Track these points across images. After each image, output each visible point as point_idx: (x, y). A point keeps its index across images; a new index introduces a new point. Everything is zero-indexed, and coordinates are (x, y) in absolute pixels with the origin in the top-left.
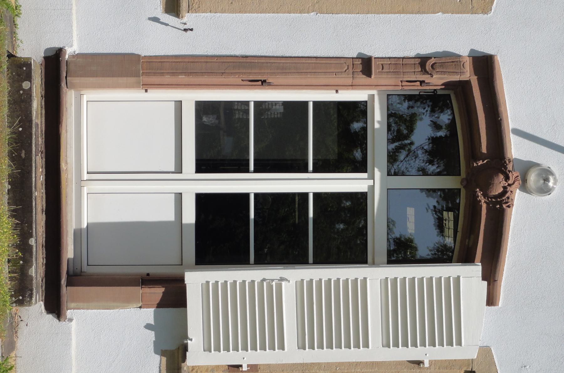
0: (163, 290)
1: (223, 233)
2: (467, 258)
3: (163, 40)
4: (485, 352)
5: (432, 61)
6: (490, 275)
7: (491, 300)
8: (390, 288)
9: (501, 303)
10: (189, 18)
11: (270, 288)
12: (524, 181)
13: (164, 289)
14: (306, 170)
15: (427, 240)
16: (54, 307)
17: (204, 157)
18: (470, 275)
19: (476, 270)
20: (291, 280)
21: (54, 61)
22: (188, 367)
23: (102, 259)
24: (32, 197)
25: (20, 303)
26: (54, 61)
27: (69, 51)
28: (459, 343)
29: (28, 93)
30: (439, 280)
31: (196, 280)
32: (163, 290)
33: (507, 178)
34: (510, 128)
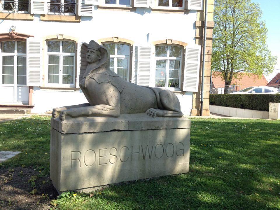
1: (22, 80)
6: (28, 37)
7: (33, 37)
8: (31, 52)
12: (14, 30)
13: (270, 103)
14: (59, 75)
15: (241, 107)
18: (28, 40)
19: (27, 39)
20: (29, 69)
22: (108, 88)
24: (256, 94)
28: (39, 42)
31: (29, 84)
33: (12, 33)
34: (196, 94)
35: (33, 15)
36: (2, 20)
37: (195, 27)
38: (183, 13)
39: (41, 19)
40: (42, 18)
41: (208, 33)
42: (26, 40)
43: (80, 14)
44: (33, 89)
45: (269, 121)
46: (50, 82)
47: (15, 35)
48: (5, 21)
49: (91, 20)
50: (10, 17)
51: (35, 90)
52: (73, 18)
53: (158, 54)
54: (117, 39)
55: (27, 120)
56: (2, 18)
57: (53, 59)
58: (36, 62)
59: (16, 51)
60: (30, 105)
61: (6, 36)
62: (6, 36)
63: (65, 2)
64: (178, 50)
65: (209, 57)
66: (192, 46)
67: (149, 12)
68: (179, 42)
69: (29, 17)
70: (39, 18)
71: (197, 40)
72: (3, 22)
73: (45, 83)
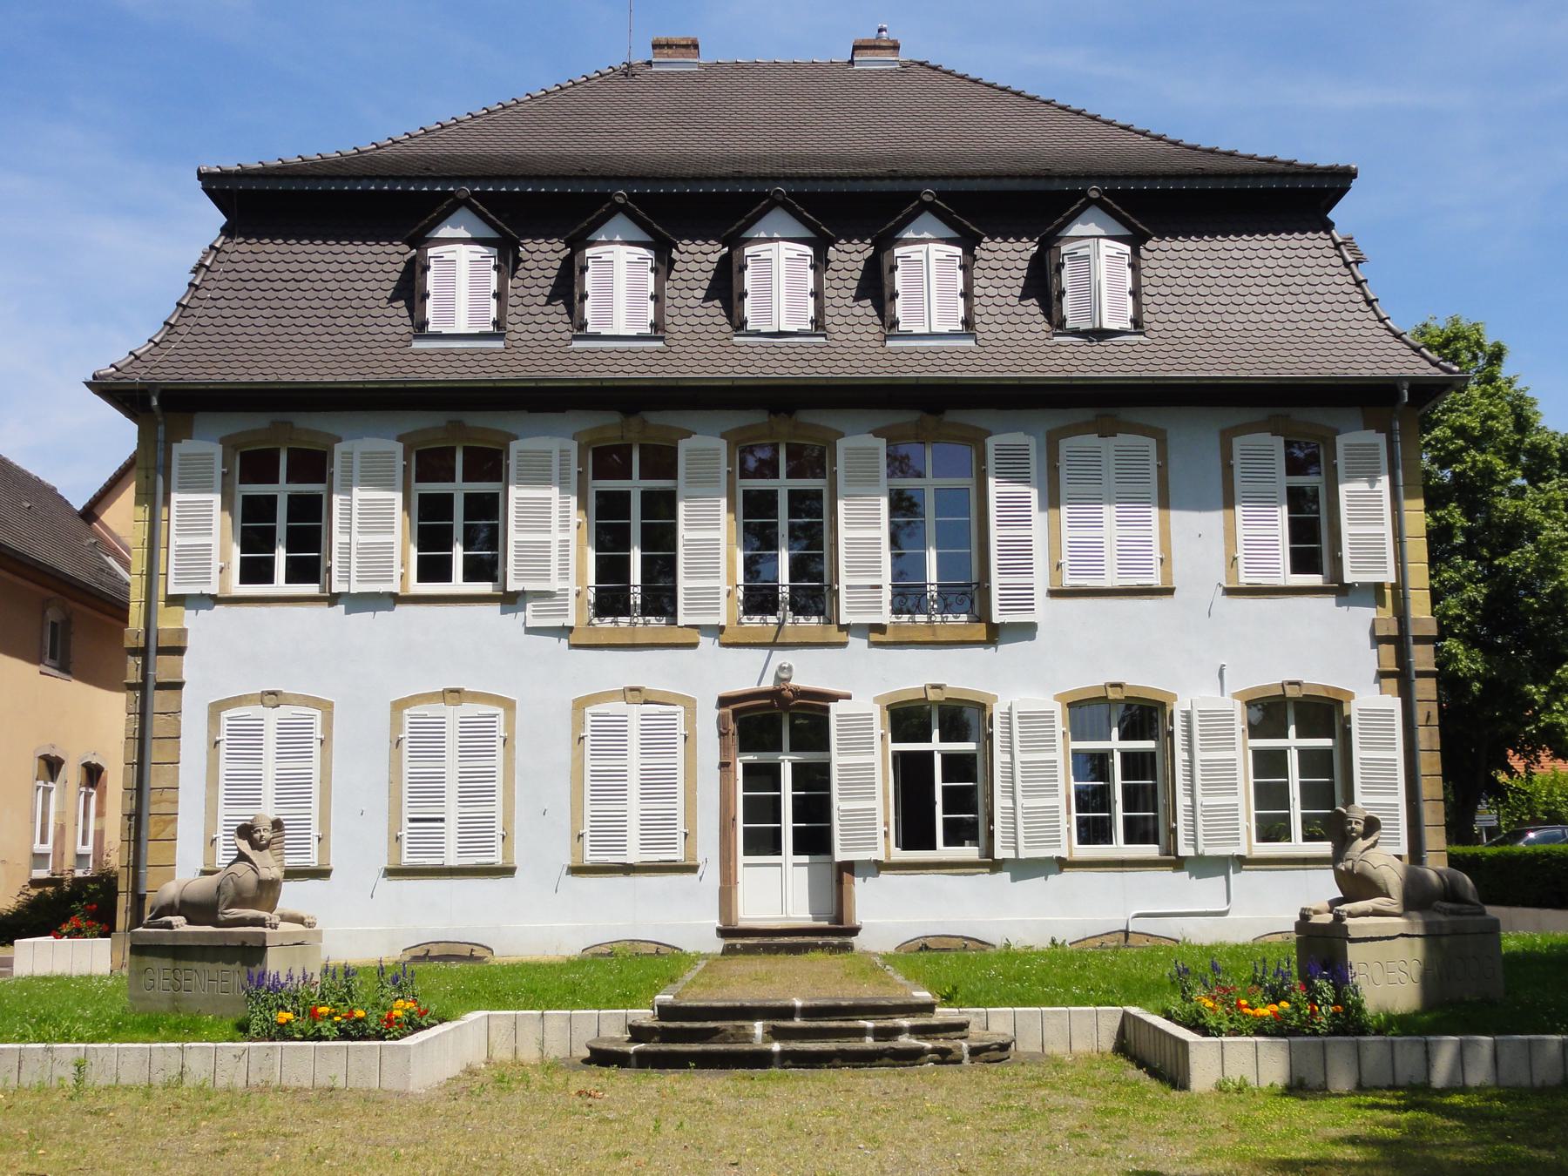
1: (814, 840)
6: (835, 698)
7: (849, 697)
8: (843, 751)
18: (835, 709)
19: (832, 705)
23: (829, 906)
31: (840, 855)
35: (843, 628)
37: (1377, 640)
39: (533, 623)
40: (875, 637)
41: (1423, 658)
42: (827, 709)
43: (997, 618)
45: (392, 1082)
46: (1083, 840)
49: (1032, 638)
52: (980, 631)
53: (1077, 733)
55: (1190, 946)
57: (1270, 763)
58: (861, 781)
64: (1322, 713)
65: (1431, 734)
66: (1373, 705)
68: (1326, 688)
69: (834, 634)
71: (1392, 683)
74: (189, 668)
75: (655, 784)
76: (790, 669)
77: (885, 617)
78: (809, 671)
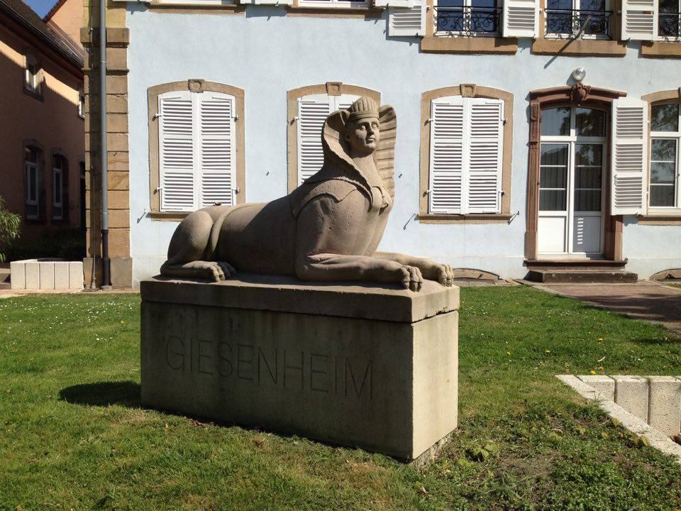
0: (617, 222)
2: (609, 105)
3: (519, 224)
4: (643, 98)
5: (532, 117)
6: (616, 95)
7: (624, 95)
9: (625, 92)
10: (512, 212)
11: (619, 182)
16: (622, 264)
17: (122, 49)
18: (617, 104)
21: (527, 264)
23: (597, 245)
25: (637, 278)
26: (527, 264)
27: (525, 259)
28: (642, 108)
29: (557, 275)
30: (510, 20)
32: (617, 222)
35: (626, 43)
36: (551, 57)
38: (364, 16)
40: (646, 50)
44: (622, 221)
47: (583, 92)
48: (559, 59)
50: (572, 48)
51: (626, 225)
52: (490, 44)
53: (655, 126)
54: (337, 87)
56: (553, 51)
59: (573, 132)
60: (616, 260)
61: (563, 96)
62: (563, 96)
63: (582, 4)
67: (142, 10)
69: (615, 47)
70: (417, 45)
72: (553, 62)
73: (645, 209)
74: (132, 58)
75: (181, 155)
76: (584, 73)
77: (654, 36)
78: (597, 74)
